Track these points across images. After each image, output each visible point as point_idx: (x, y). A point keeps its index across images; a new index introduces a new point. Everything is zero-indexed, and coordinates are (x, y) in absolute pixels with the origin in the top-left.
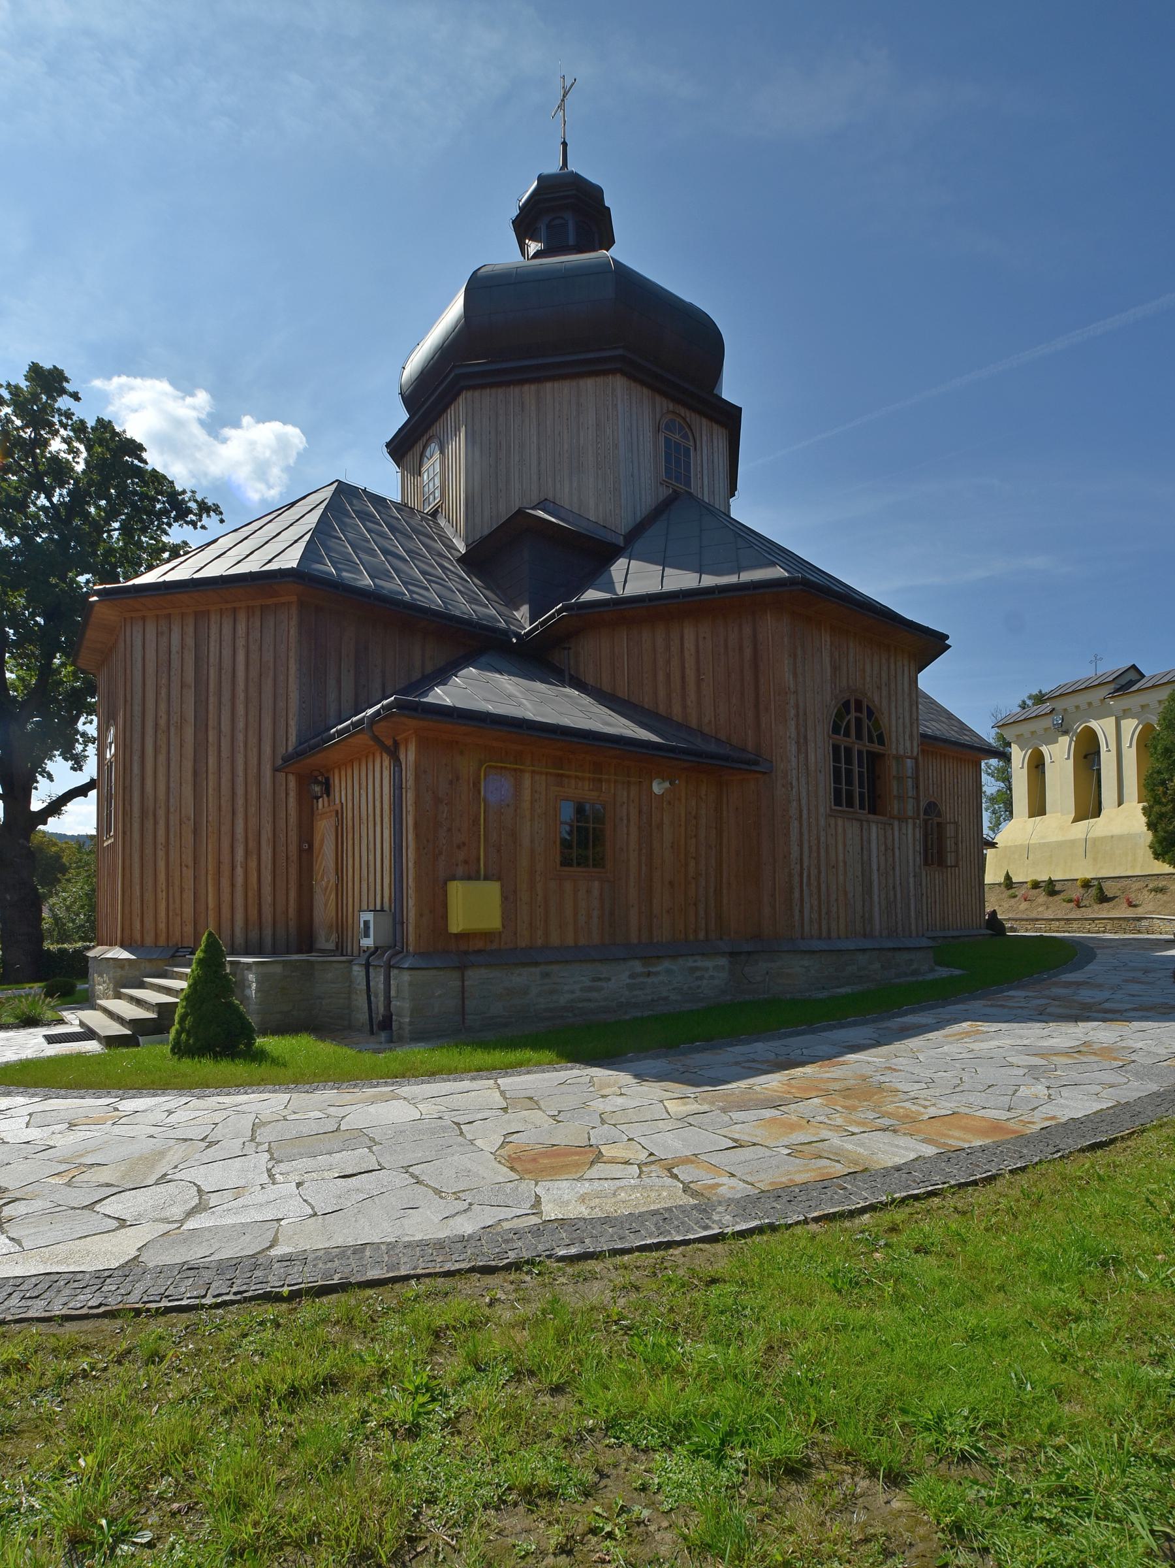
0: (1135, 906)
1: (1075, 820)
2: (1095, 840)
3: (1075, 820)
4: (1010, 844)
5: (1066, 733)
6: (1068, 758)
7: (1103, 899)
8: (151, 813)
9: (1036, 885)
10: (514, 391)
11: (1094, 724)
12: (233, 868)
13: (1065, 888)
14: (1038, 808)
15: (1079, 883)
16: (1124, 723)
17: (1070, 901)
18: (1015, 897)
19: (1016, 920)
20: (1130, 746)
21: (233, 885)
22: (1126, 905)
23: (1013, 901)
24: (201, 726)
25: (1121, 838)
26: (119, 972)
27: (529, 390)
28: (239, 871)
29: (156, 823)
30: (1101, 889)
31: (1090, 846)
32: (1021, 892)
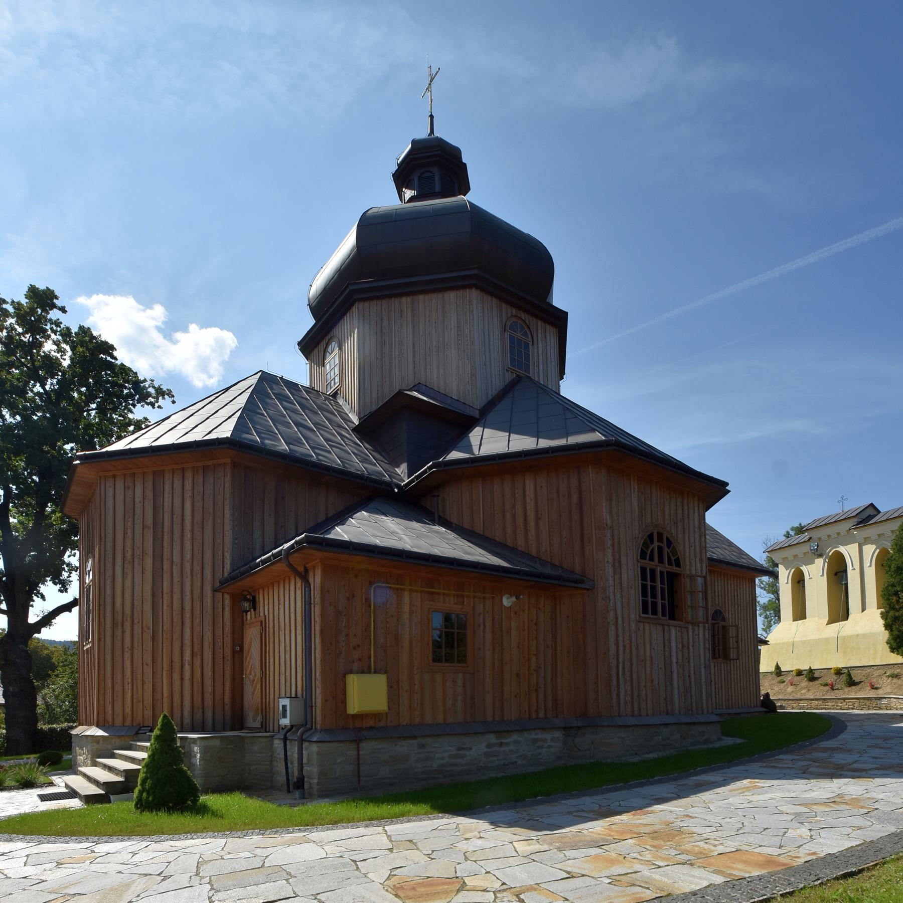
0: (876, 688)
1: (829, 623)
2: (844, 638)
3: (829, 623)
4: (779, 641)
5: (820, 556)
6: (823, 575)
7: (851, 683)
8: (120, 625)
9: (799, 673)
10: (395, 302)
11: (842, 549)
12: (182, 666)
13: (822, 675)
14: (800, 613)
15: (832, 671)
16: (865, 548)
17: (826, 685)
18: (784, 682)
19: (784, 700)
20: (870, 566)
21: (182, 679)
22: (869, 688)
23: (782, 685)
24: (158, 558)
25: (864, 636)
26: (96, 746)
27: (406, 301)
28: (187, 668)
29: (123, 632)
30: (850, 676)
31: (840, 643)
32: (788, 679)
